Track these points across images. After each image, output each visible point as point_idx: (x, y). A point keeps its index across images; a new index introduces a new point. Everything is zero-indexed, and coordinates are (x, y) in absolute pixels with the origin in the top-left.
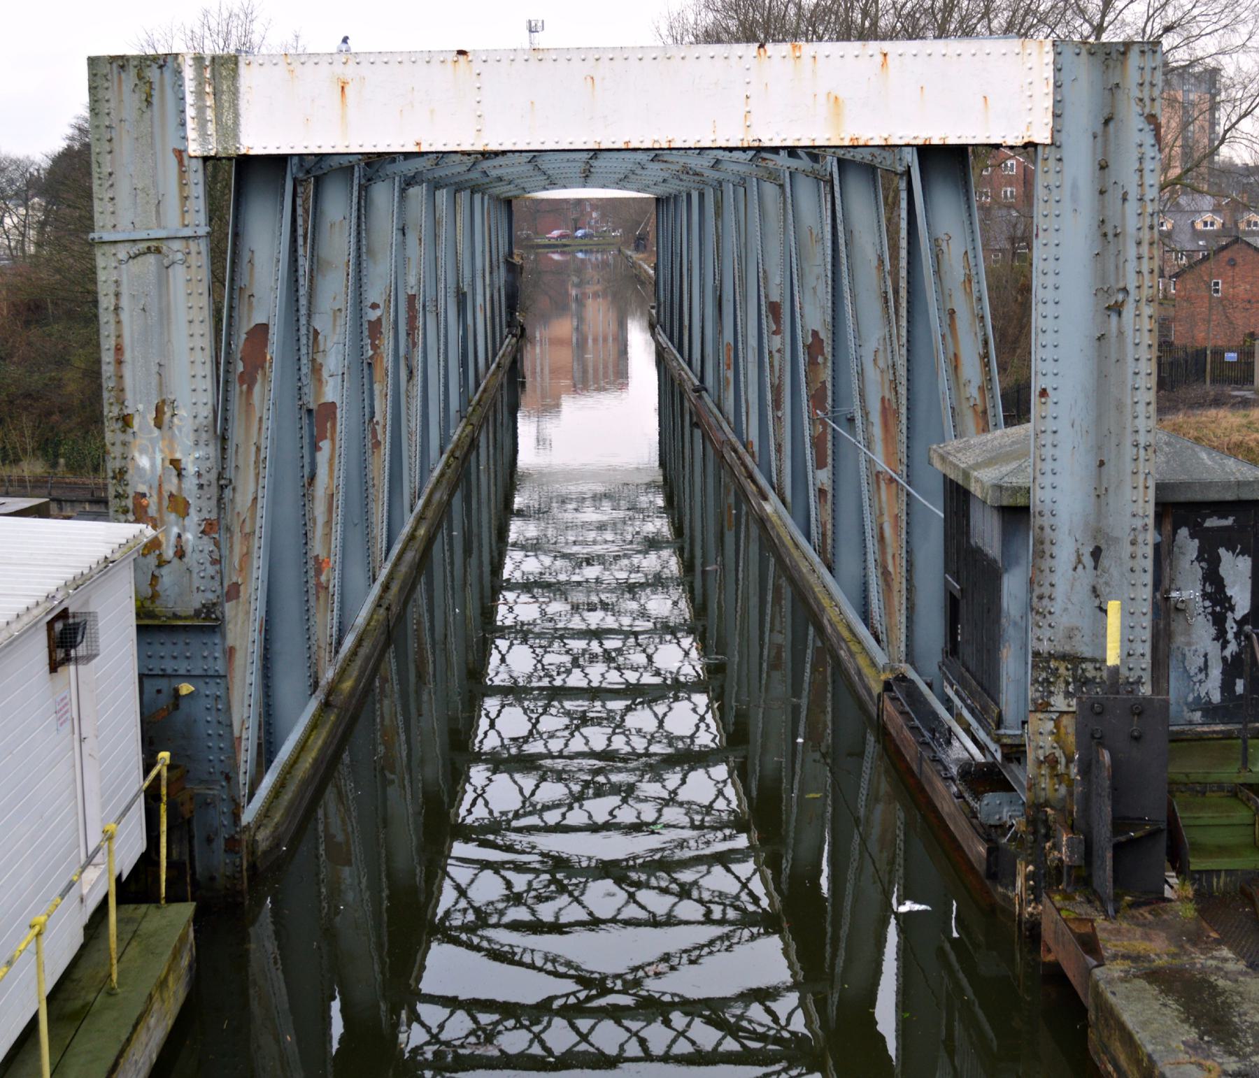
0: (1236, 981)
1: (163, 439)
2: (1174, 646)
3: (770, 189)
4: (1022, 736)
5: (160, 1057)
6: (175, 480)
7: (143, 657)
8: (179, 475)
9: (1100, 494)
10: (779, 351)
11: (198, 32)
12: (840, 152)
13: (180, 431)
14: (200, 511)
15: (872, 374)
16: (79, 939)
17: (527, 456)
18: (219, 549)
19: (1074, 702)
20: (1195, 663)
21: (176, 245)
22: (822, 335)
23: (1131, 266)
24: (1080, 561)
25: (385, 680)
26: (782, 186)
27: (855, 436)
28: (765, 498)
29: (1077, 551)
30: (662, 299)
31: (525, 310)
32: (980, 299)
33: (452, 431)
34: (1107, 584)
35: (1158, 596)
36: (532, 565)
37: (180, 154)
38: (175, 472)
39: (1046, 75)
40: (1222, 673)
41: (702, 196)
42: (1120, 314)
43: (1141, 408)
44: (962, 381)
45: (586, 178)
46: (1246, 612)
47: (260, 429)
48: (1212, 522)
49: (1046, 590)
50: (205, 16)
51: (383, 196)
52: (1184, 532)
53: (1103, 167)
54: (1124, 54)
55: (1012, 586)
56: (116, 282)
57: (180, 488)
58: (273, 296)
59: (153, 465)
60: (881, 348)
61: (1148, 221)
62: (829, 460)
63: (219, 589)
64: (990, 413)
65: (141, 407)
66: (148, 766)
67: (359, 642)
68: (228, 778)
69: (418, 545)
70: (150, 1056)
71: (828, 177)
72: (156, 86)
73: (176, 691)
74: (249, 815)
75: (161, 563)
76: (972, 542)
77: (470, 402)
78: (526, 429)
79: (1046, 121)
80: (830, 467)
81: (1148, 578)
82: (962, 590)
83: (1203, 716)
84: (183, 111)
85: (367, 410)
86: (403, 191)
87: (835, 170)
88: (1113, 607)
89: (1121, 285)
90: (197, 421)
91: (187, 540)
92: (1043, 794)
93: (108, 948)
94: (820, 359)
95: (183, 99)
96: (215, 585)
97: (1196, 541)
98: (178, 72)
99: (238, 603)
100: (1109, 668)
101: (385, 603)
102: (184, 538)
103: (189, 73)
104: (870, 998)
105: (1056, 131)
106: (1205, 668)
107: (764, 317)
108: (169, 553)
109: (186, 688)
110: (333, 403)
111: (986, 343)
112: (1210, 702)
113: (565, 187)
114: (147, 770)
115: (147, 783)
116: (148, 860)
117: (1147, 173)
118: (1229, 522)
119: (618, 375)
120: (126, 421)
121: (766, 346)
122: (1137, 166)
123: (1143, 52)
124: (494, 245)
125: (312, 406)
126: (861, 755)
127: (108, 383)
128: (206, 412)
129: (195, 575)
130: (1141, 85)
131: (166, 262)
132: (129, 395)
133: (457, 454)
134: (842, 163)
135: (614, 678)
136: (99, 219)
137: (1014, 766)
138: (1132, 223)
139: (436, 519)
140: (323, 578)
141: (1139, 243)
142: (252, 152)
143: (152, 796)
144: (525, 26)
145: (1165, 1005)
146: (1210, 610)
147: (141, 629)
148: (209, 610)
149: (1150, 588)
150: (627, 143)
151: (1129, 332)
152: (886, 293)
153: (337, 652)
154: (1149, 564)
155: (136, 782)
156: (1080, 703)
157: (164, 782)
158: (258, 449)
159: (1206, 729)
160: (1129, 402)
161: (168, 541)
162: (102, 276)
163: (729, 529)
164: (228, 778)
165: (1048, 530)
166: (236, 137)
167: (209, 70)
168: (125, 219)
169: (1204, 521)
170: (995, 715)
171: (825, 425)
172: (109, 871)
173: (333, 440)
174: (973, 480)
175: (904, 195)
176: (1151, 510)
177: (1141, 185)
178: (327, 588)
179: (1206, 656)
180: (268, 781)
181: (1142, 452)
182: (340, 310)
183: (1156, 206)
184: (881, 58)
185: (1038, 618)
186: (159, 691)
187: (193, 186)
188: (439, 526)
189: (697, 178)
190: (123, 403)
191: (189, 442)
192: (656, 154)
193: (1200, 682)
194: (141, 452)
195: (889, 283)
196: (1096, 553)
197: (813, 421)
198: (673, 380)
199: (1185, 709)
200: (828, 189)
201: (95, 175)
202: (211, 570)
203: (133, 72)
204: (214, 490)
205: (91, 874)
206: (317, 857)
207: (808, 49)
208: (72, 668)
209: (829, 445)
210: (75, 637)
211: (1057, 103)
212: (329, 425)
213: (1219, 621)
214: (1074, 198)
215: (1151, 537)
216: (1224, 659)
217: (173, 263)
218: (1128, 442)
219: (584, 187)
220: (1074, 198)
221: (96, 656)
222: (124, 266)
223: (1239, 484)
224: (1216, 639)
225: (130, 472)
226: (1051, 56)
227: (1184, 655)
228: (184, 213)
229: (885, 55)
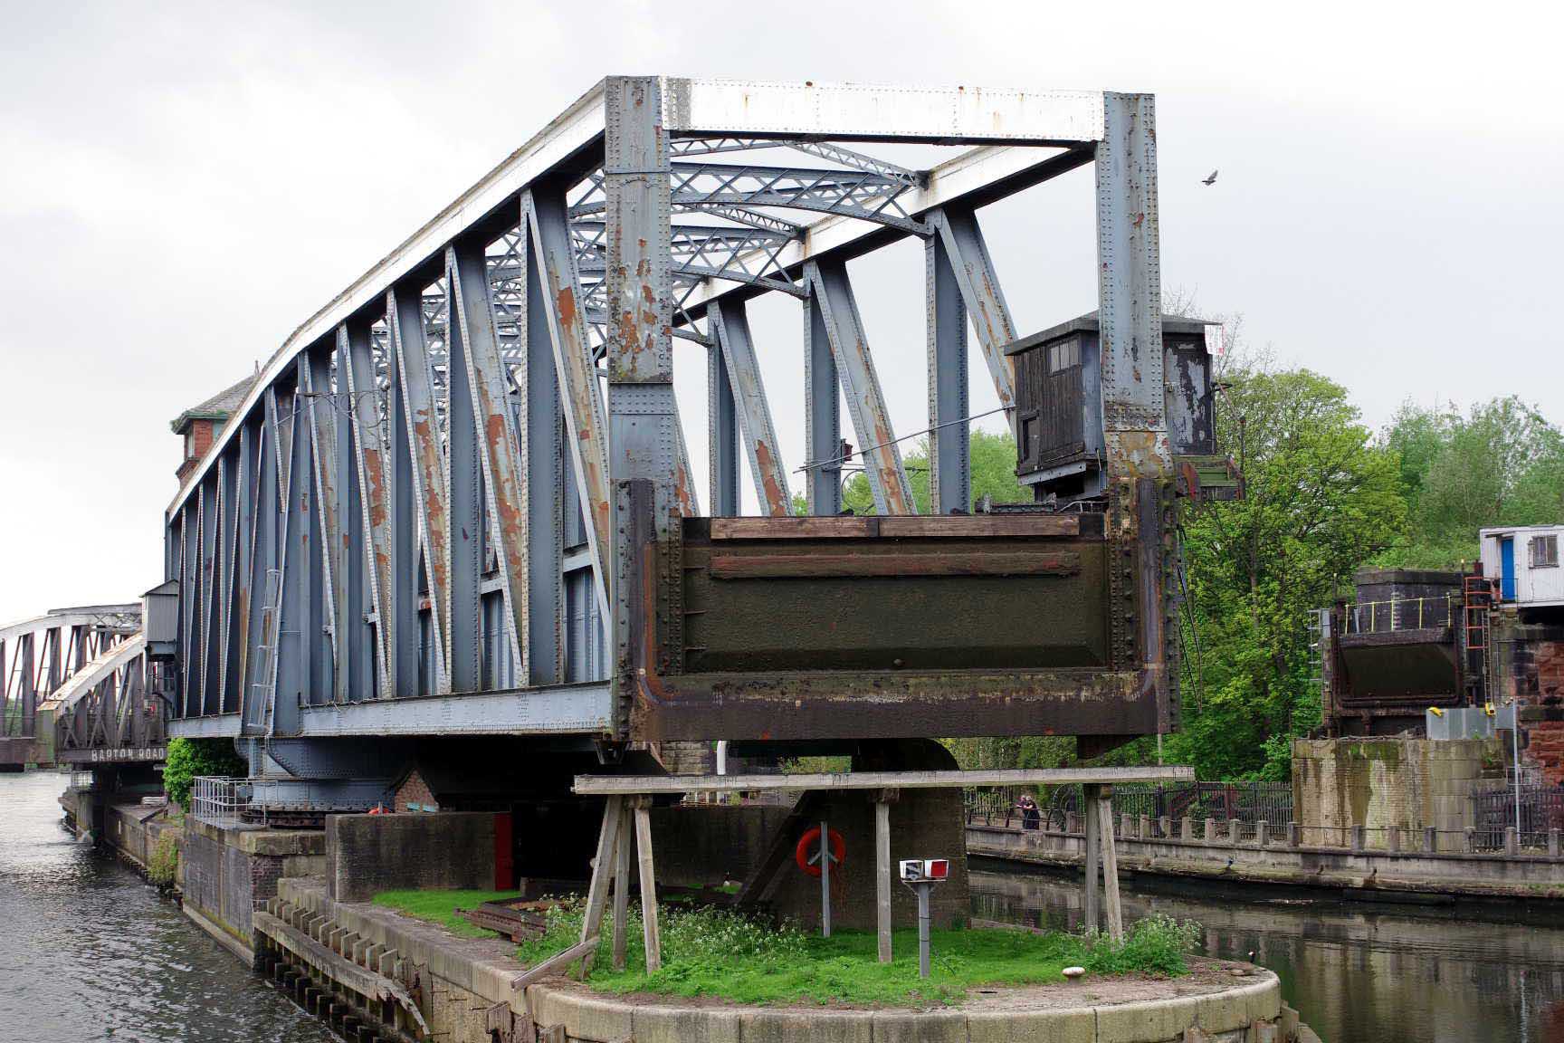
9: (1135, 318)
21: (653, 176)
59: (635, 296)
84: (660, 106)
103: (664, 86)
105: (1106, 135)
112: (1187, 443)
151: (1145, 234)
158: (582, 360)
166: (688, 120)
173: (505, 436)
194: (630, 288)
212: (500, 428)
213: (1190, 399)
214: (1116, 168)
220: (1116, 168)
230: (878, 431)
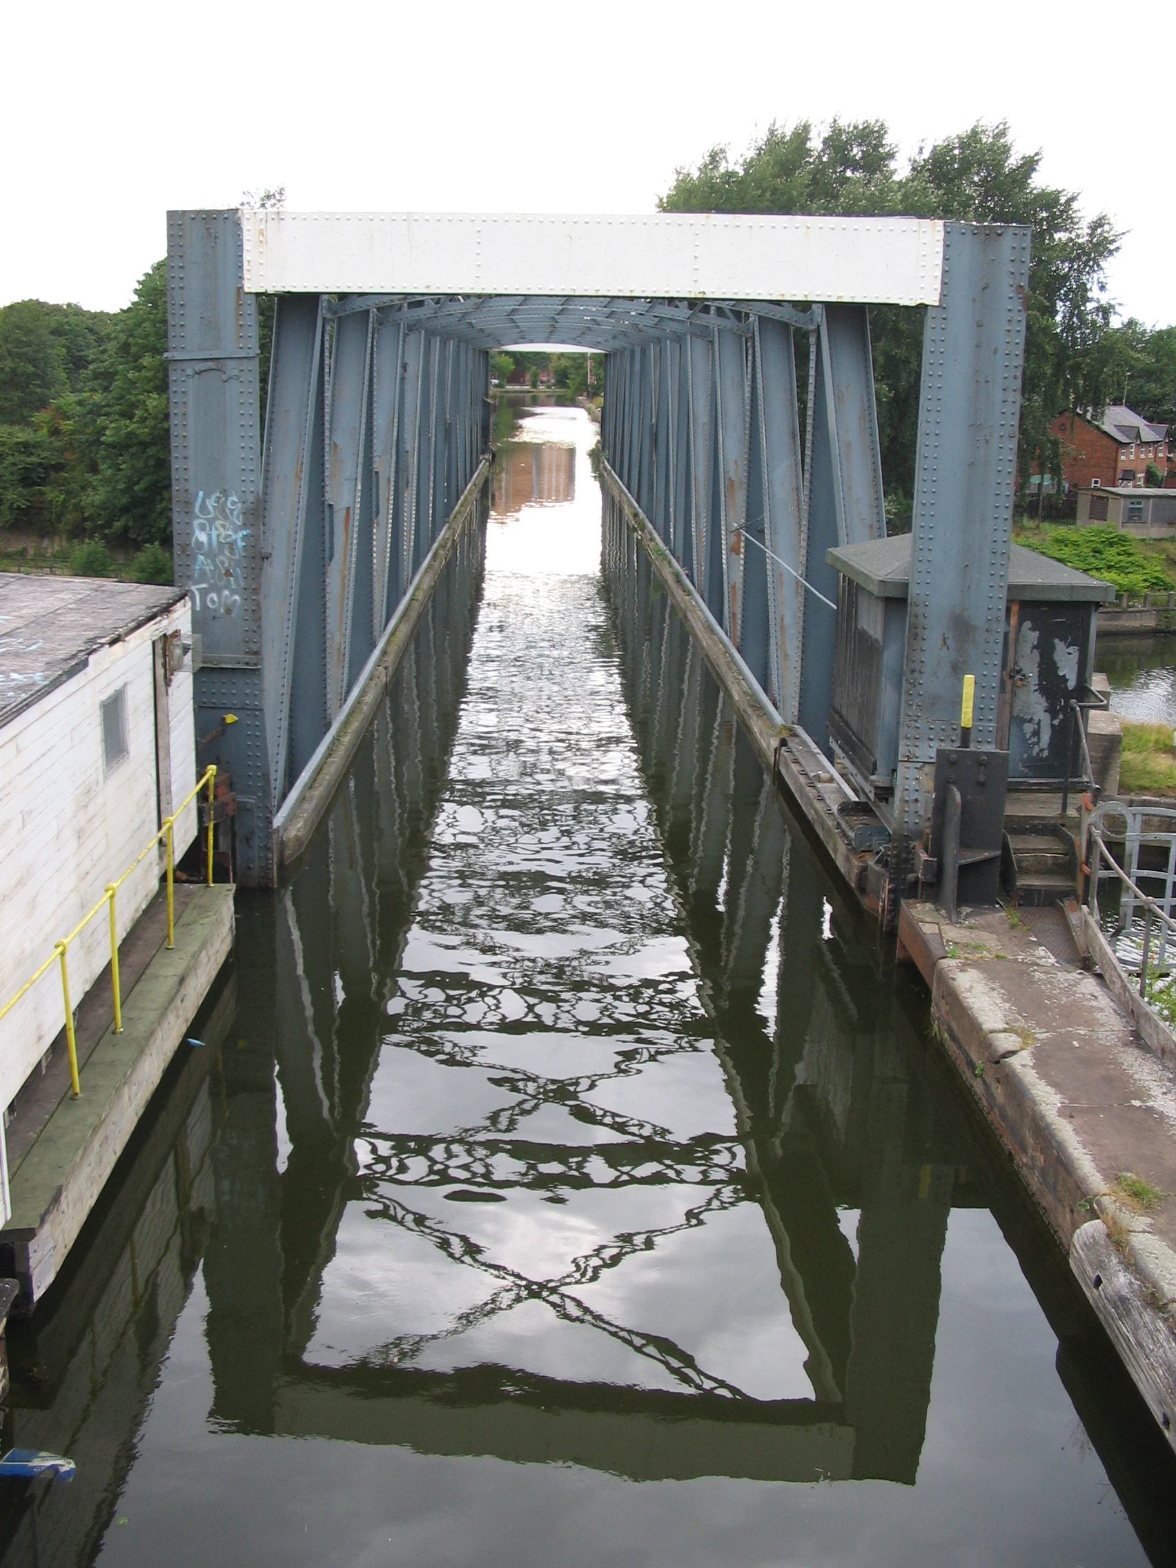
41: (644, 352)
49: (916, 666)
66: (200, 775)
73: (224, 719)
74: (278, 821)
76: (859, 626)
78: (492, 528)
88: (969, 679)
90: (246, 506)
105: (943, 295)
109: (230, 718)
113: (532, 342)
131: (224, 377)
137: (882, 804)
149: (999, 668)
216: (1053, 726)
223: (1072, 588)
226: (942, 234)
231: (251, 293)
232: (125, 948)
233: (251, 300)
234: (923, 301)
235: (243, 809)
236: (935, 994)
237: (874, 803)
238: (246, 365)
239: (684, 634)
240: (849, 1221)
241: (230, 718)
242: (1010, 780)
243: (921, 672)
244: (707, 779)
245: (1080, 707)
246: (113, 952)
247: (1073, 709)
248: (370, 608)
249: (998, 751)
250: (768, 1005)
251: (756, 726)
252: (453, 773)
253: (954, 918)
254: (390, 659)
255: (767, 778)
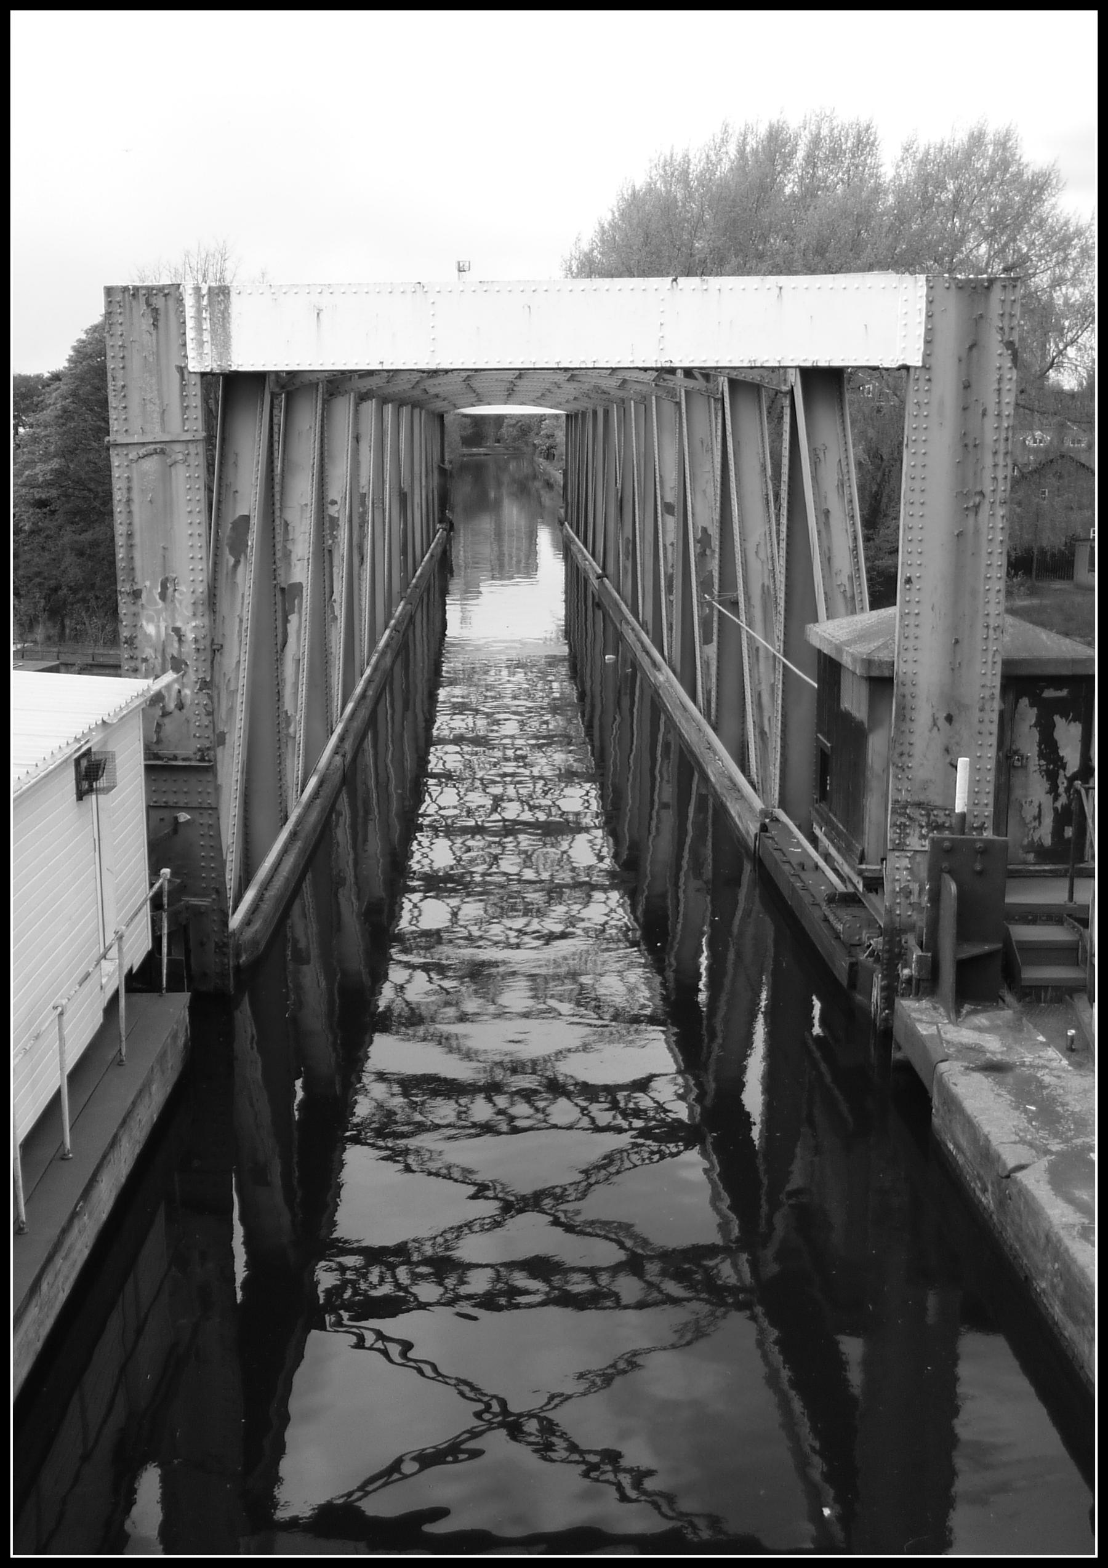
0: (1059, 1077)
1: (166, 609)
2: (1013, 798)
3: (668, 407)
4: (881, 870)
5: (160, 1118)
6: (176, 645)
7: (150, 791)
8: (180, 640)
10: (672, 544)
11: (181, 271)
12: (734, 374)
13: (180, 604)
14: (197, 671)
15: (755, 565)
16: (99, 1019)
17: (453, 630)
18: (212, 703)
19: (927, 843)
20: (1030, 812)
21: (178, 447)
22: (710, 532)
23: (988, 474)
24: (935, 724)
25: (340, 814)
26: (678, 404)
27: (738, 618)
28: (659, 670)
29: (933, 715)
30: (569, 500)
31: (452, 511)
32: (851, 501)
33: (393, 609)
34: (958, 744)
35: (1001, 754)
36: (460, 724)
37: (182, 370)
38: (176, 638)
39: (919, 307)
40: (1054, 822)
41: (606, 413)
42: (976, 513)
43: (992, 595)
44: (834, 570)
45: (510, 395)
46: (1076, 770)
47: (243, 604)
48: (1049, 693)
49: (906, 748)
50: (187, 256)
51: (343, 408)
52: (1024, 702)
53: (967, 386)
54: (988, 288)
55: (877, 744)
56: (128, 478)
57: (180, 651)
58: (253, 492)
60: (762, 542)
61: (1003, 435)
62: (715, 638)
63: (212, 736)
64: (858, 599)
65: (148, 584)
67: (321, 784)
68: (217, 892)
69: (369, 703)
70: (152, 1116)
71: (719, 396)
72: (162, 312)
73: (176, 818)
74: (235, 921)
75: (165, 714)
77: (408, 584)
78: (453, 612)
79: (917, 346)
80: (715, 643)
81: (993, 740)
82: (831, 747)
83: (1035, 857)
85: (327, 590)
86: (357, 405)
87: (726, 389)
88: (963, 763)
89: (978, 489)
91: (186, 695)
92: (898, 919)
93: (119, 1028)
94: (708, 552)
95: (184, 323)
96: (209, 733)
97: (1035, 709)
98: (180, 301)
99: (224, 748)
100: (958, 815)
101: (342, 751)
102: (183, 693)
103: (189, 301)
104: (740, 1086)
105: (927, 356)
106: (1039, 817)
107: (659, 515)
108: (171, 705)
109: (184, 817)
110: (301, 584)
111: (855, 539)
113: (489, 404)
114: (152, 885)
115: (151, 894)
116: (152, 958)
117: (1004, 393)
118: (1064, 693)
119: (528, 566)
120: (136, 594)
121: (661, 539)
122: (996, 386)
123: (1004, 287)
124: (429, 451)
125: (283, 585)
126: (738, 883)
127: (120, 565)
128: (201, 588)
129: (192, 725)
130: (1002, 315)
132: (138, 574)
133: (399, 628)
134: (732, 382)
135: (527, 816)
136: (114, 426)
137: (872, 896)
138: (990, 436)
139: (383, 683)
140: (291, 730)
141: (995, 453)
142: (241, 369)
143: (156, 903)
144: (455, 266)
145: (999, 1095)
146: (1044, 768)
147: (149, 769)
148: (203, 753)
150: (558, 363)
151: (984, 529)
152: (767, 495)
153: (302, 791)
154: (994, 728)
155: (143, 892)
156: (933, 842)
157: (165, 893)
158: (241, 621)
159: (1037, 868)
160: (982, 589)
161: (170, 695)
162: (116, 473)
163: (626, 694)
164: (217, 892)
165: (909, 697)
167: (206, 298)
168: (136, 424)
169: (1042, 692)
170: (859, 853)
171: (711, 607)
172: (120, 966)
174: (845, 654)
175: (787, 411)
176: (997, 682)
177: (999, 403)
178: (295, 738)
179: (1040, 806)
180: (250, 895)
181: (991, 632)
182: (306, 505)
183: (1011, 422)
184: (778, 290)
185: (898, 771)
186: (162, 820)
187: (192, 398)
188: (384, 688)
189: (605, 396)
190: (133, 580)
191: (188, 613)
192: (572, 374)
193: (1034, 828)
194: (150, 620)
195: (770, 487)
196: (949, 719)
197: (701, 604)
198: (578, 568)
199: (1021, 851)
200: (719, 406)
201: (110, 388)
202: (206, 721)
203: (142, 300)
204: (208, 654)
205: (108, 966)
206: (285, 956)
207: (714, 282)
208: (94, 797)
209: (715, 625)
210: (98, 772)
211: (929, 331)
212: (296, 602)
213: (1052, 777)
215: (997, 705)
216: (1055, 809)
217: (176, 462)
218: (980, 622)
219: (506, 404)
221: (114, 787)
222: (134, 465)
224: (1049, 792)
225: (140, 637)
227: (1022, 806)
228: (184, 421)
229: (781, 288)
230: (764, 592)
231: (195, 373)
232: (75, 1076)
233: (196, 380)
234: (905, 362)
235: (198, 913)
236: (936, 1101)
237: (863, 894)
238: (192, 449)
239: (657, 707)
240: (852, 1348)
241: (184, 817)
242: (1010, 867)
243: (910, 756)
244: (703, 1035)
245: (1085, 788)
246: (62, 1079)
247: (1078, 792)
248: (328, 687)
249: (996, 837)
250: (753, 1099)
251: (733, 809)
252: (404, 924)
253: (953, 1016)
254: (348, 746)
255: (748, 867)
